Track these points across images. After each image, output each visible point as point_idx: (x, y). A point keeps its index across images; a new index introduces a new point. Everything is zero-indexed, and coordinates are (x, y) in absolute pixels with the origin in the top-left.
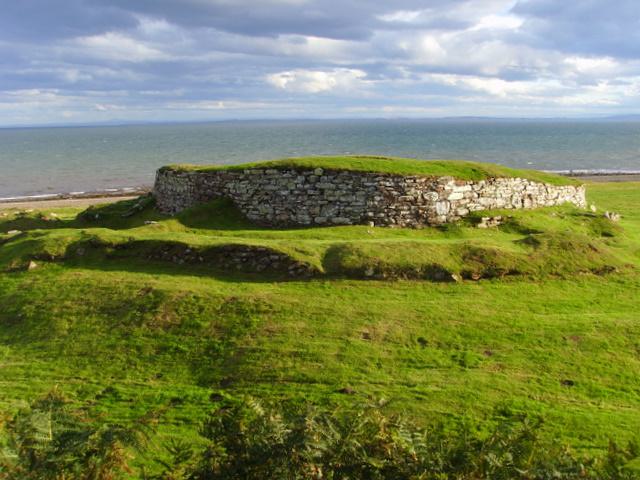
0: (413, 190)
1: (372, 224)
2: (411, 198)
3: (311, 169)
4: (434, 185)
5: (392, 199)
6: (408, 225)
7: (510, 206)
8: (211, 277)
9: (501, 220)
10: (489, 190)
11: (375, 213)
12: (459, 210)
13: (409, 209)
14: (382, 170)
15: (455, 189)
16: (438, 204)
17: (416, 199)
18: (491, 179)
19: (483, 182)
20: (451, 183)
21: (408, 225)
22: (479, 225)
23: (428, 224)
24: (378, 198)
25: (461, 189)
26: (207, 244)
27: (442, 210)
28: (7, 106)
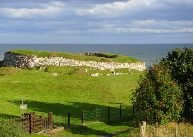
0: (25, 59)
1: (16, 67)
2: (25, 61)
3: (11, 52)
4: (30, 58)
5: (20, 60)
6: (24, 68)
7: (54, 65)
8: (94, 134)
9: (46, 68)
10: (48, 60)
11: (17, 64)
12: (37, 65)
13: (24, 64)
14: (20, 54)
15: (37, 59)
16: (31, 63)
17: (26, 61)
18: (49, 56)
19: (46, 57)
20: (35, 57)
21: (24, 68)
22: (39, 69)
23: (28, 68)
24: (18, 60)
25: (39, 59)
26: (57, 103)
27: (32, 64)
28: (190, 30)
